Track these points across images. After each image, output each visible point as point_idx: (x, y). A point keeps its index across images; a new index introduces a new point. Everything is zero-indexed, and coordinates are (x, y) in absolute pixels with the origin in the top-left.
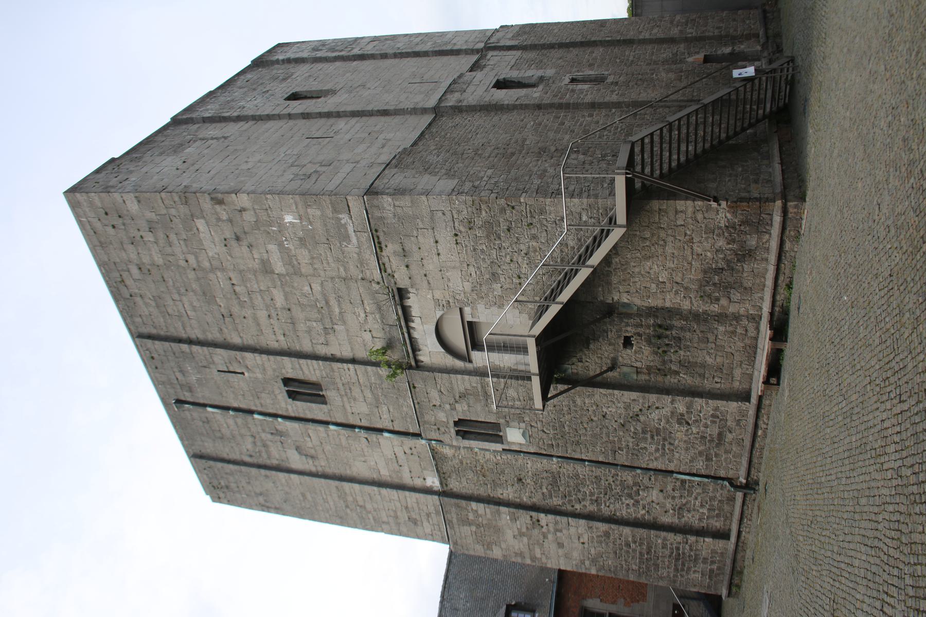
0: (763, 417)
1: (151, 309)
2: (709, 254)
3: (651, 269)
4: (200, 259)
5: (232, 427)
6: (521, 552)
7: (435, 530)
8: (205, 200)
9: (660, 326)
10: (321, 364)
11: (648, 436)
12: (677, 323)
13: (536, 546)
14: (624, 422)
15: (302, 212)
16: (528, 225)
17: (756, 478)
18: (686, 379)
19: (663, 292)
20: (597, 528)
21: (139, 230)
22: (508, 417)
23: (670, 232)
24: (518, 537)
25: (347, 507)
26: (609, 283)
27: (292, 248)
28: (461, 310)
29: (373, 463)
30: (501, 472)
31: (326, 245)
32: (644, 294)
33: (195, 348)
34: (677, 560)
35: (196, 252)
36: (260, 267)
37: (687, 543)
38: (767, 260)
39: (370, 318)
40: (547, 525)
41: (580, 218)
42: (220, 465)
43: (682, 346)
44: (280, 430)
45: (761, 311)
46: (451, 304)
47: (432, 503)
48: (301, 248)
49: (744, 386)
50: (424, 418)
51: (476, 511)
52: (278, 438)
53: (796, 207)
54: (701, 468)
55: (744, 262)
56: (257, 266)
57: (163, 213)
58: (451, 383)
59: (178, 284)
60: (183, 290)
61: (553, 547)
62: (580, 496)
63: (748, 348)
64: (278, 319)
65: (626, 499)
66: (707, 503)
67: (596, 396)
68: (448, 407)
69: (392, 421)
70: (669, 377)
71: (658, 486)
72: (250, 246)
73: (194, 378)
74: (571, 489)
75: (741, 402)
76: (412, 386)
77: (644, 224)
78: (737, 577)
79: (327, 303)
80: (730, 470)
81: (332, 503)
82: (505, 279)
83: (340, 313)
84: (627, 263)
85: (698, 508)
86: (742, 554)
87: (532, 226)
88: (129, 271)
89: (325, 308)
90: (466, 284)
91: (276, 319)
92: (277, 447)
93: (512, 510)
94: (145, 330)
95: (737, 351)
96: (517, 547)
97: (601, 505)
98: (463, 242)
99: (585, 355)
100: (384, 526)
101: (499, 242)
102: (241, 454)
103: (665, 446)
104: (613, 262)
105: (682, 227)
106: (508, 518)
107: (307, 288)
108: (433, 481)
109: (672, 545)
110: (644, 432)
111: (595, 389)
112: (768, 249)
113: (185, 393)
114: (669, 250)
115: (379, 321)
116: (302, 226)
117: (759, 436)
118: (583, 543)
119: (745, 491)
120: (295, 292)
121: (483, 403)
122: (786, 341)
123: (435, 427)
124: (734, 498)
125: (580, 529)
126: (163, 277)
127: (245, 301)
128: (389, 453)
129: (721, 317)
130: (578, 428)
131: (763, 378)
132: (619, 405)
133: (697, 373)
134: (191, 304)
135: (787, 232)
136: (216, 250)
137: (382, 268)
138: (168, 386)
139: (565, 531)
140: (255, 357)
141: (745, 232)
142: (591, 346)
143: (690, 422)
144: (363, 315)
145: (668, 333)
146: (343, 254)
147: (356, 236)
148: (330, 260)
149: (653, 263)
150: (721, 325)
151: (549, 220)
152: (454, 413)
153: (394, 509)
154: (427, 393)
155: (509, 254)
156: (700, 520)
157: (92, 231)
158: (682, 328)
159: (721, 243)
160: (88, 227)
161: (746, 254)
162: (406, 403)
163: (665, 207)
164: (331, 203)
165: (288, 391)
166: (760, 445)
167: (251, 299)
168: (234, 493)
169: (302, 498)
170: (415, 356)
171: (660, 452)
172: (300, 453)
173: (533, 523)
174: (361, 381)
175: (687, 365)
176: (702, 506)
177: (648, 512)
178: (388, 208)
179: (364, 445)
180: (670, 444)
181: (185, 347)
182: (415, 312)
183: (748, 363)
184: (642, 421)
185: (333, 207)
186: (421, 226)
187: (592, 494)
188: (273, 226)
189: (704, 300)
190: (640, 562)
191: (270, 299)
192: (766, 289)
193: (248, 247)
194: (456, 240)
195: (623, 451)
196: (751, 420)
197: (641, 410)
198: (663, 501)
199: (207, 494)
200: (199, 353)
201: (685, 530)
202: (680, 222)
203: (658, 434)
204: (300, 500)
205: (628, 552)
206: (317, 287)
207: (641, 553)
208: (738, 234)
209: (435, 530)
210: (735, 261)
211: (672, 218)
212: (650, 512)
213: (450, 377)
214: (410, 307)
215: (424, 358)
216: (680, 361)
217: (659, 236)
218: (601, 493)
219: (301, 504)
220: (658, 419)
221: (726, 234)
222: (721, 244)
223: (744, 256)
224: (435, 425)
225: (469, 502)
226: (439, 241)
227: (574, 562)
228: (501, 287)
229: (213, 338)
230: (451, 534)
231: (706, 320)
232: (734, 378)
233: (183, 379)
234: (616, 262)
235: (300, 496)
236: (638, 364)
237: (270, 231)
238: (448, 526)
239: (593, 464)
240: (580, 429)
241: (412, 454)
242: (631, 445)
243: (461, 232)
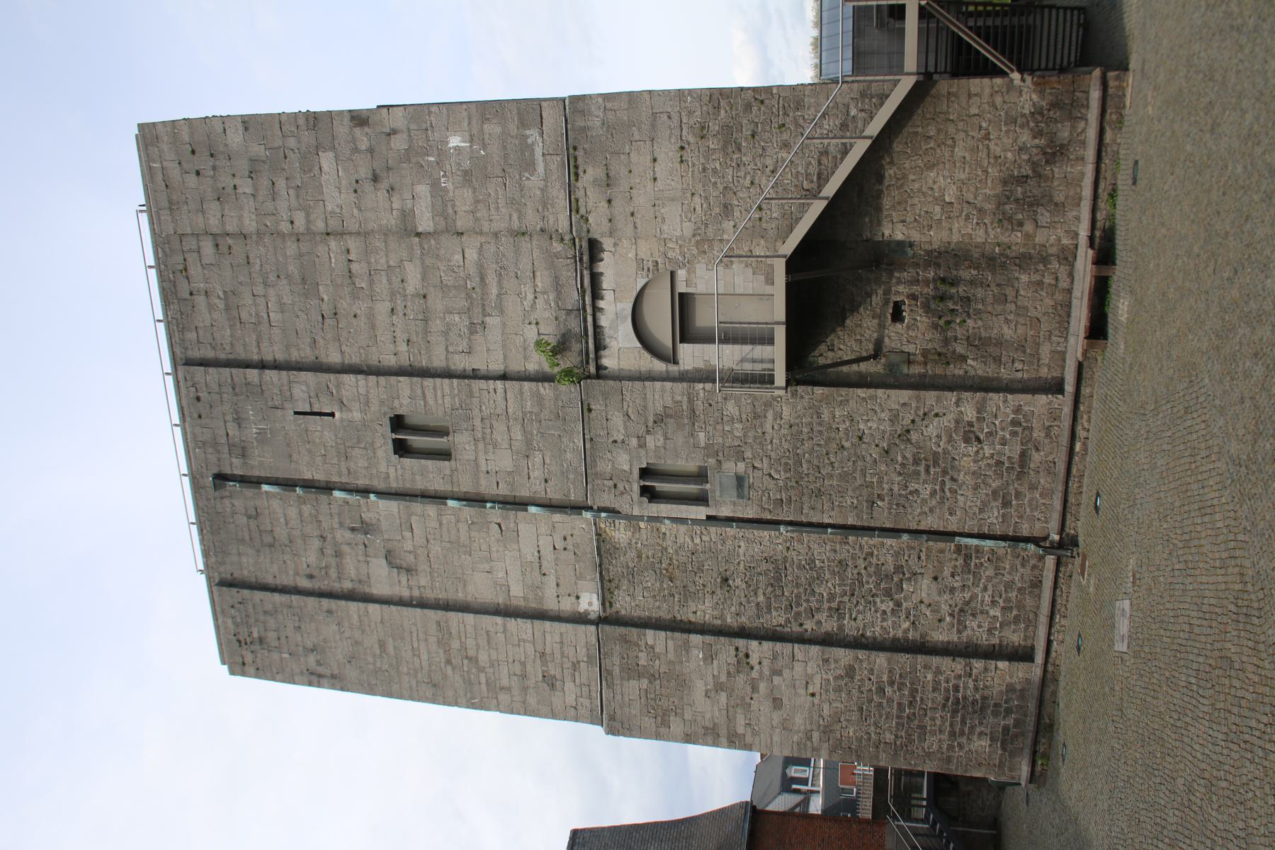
0: (1082, 417)
1: (216, 315)
2: (1009, 155)
3: (935, 182)
4: (313, 217)
6: (714, 724)
7: (581, 697)
8: (342, 120)
9: (943, 280)
11: (922, 468)
12: (966, 274)
15: (475, 131)
16: (779, 128)
17: (1072, 532)
18: (975, 367)
19: (949, 217)
21: (234, 175)
22: (721, 454)
23: (961, 125)
24: (713, 694)
25: (449, 662)
26: (879, 209)
27: (450, 187)
28: (673, 274)
29: (501, 574)
30: (698, 569)
31: (500, 179)
32: (925, 223)
33: (270, 375)
34: (955, 712)
35: (310, 206)
37: (970, 675)
38: (1083, 159)
39: (540, 302)
40: (760, 663)
42: (259, 595)
43: (971, 311)
44: (368, 520)
45: (1077, 239)
46: (660, 266)
48: (464, 186)
49: (1054, 374)
50: (595, 466)
52: (360, 537)
53: (1118, 78)
54: (995, 521)
55: (1055, 163)
56: (393, 222)
57: (277, 145)
58: (645, 398)
60: (272, 278)
61: (766, 707)
62: (814, 605)
63: (1059, 308)
64: (405, 314)
65: (882, 602)
66: (1001, 596)
67: (851, 402)
68: (634, 441)
69: (546, 481)
70: (952, 366)
71: (930, 573)
73: (255, 430)
74: (801, 590)
75: (1052, 394)
76: (585, 408)
77: (928, 116)
78: (1044, 737)
79: (482, 279)
80: (1036, 522)
81: (425, 657)
82: (741, 213)
83: (499, 295)
84: (905, 176)
85: (988, 608)
86: (1052, 687)
87: (784, 129)
88: (199, 252)
89: (477, 290)
91: (401, 314)
92: (357, 555)
93: (709, 639)
94: (196, 354)
95: (1044, 314)
96: (708, 716)
97: (844, 619)
98: (690, 159)
99: (839, 338)
100: (504, 697)
101: (739, 156)
102: (297, 574)
103: (945, 485)
104: (887, 175)
105: (978, 117)
106: (701, 656)
108: (590, 602)
109: (948, 682)
110: (916, 462)
111: (851, 389)
112: (1083, 143)
113: (234, 460)
114: (959, 152)
115: (552, 305)
116: (472, 152)
117: (1078, 453)
118: (813, 695)
119: (1059, 552)
120: (439, 264)
122: (1114, 263)
123: (611, 483)
124: (1041, 581)
125: (810, 664)
126: (248, 257)
127: (362, 288)
128: (529, 552)
129: (1024, 261)
130: (821, 465)
131: (1085, 332)
132: (883, 415)
133: (990, 355)
135: (1108, 117)
136: (339, 201)
137: (574, 206)
138: (210, 450)
139: (786, 673)
141: (1056, 119)
142: (848, 322)
143: (982, 437)
144: (530, 297)
145: (953, 291)
147: (545, 161)
148: (502, 202)
149: (938, 174)
150: (1024, 273)
151: (806, 117)
152: (643, 452)
153: (523, 659)
154: (607, 420)
155: (749, 173)
156: (990, 631)
157: (164, 183)
158: (972, 283)
159: (1025, 137)
160: (159, 177)
161: (1056, 152)
162: (571, 445)
163: (955, 90)
164: (519, 113)
165: (394, 440)
166: (1078, 470)
167: (371, 282)
168: (269, 651)
169: (378, 652)
170: (597, 358)
172: (390, 564)
173: (738, 662)
175: (980, 344)
177: (913, 623)
178: (596, 113)
180: (953, 479)
181: (253, 374)
182: (607, 283)
183: (1059, 334)
184: (913, 441)
185: (519, 119)
186: (637, 137)
187: (832, 597)
188: (431, 155)
189: (1003, 226)
190: (897, 724)
191: (399, 279)
192: (1083, 203)
193: (388, 191)
194: (681, 157)
196: (1066, 423)
197: (913, 421)
198: (937, 598)
199: (223, 662)
200: (272, 383)
201: (969, 651)
202: (974, 110)
203: (936, 463)
204: (374, 656)
205: (880, 704)
206: (472, 255)
207: (900, 704)
208: (1046, 123)
210: (1043, 163)
211: (964, 104)
212: (917, 623)
213: (644, 387)
214: (602, 274)
215: (609, 361)
216: (969, 337)
217: (947, 132)
218: (846, 594)
219: (374, 664)
220: (937, 436)
221: (1032, 124)
222: (1025, 139)
223: (1054, 154)
224: (611, 479)
225: (642, 630)
226: (659, 160)
227: (796, 738)
228: (734, 226)
229: (299, 359)
231: (1003, 266)
232: (1042, 362)
233: (237, 433)
234: (890, 175)
235: (376, 646)
236: (910, 348)
237: (423, 163)
238: (604, 683)
241: (565, 549)
242: (896, 488)
243: (689, 143)
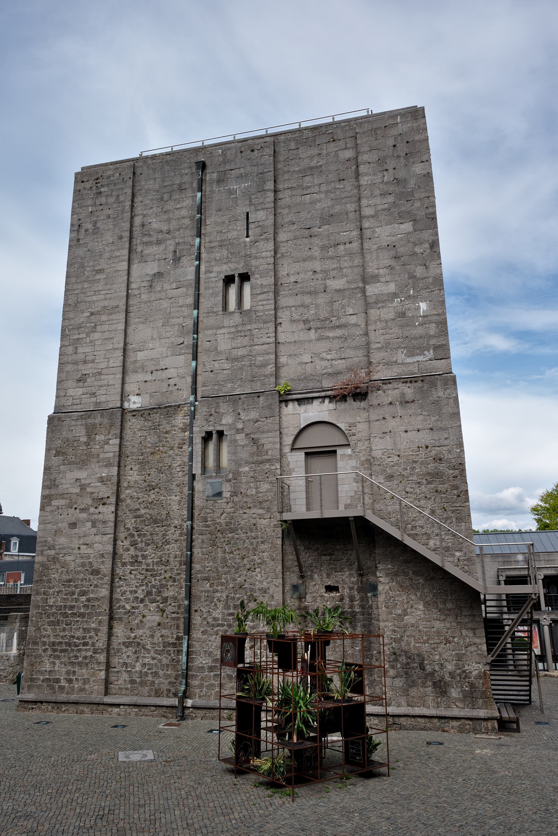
5: (177, 212)
6: (58, 486)
7: (73, 399)
10: (271, 312)
13: (67, 501)
14: (246, 588)
20: (103, 562)
22: (235, 481)
24: (78, 484)
27: (395, 304)
36: (371, 273)
51: (107, 443)
56: (370, 270)
59: (338, 193)
72: (390, 267)
90: (380, 453)
92: (159, 254)
107: (351, 312)
118: (79, 548)
121: (251, 460)
125: (100, 545)
134: (320, 201)
140: (270, 251)
146: (395, 349)
147: (414, 363)
153: (96, 361)
159: (450, 667)
171: (214, 622)
172: (154, 275)
174: (256, 347)
176: (144, 665)
179: (173, 339)
189: (391, 655)
193: (390, 266)
195: (210, 587)
209: (73, 399)
227: (50, 539)
238: (82, 413)
239: (189, 559)
240: (230, 547)
241: (169, 385)
242: (218, 595)
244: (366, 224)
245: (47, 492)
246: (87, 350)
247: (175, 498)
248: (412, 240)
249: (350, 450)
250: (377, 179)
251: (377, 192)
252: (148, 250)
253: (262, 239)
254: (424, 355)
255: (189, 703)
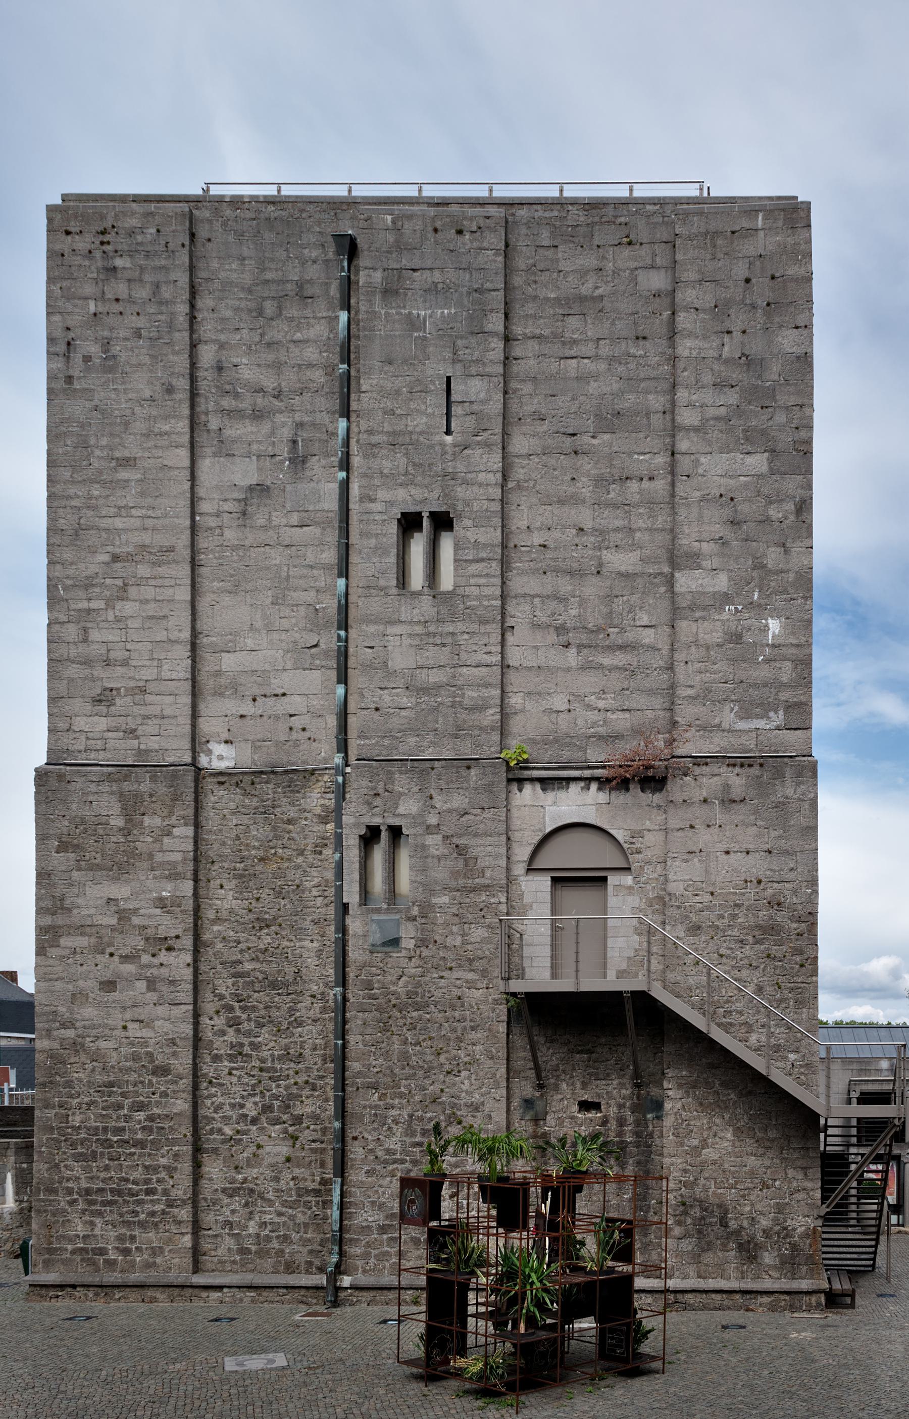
7: (87, 738)
14: (444, 1103)
22: (423, 921)
25: (116, 558)
27: (725, 616)
39: (593, 716)
41: (792, 1051)
47: (168, 746)
69: (377, 709)
90: (681, 886)
107: (645, 620)
114: (752, 1161)
118: (125, 1028)
140: (495, 472)
147: (750, 731)
148: (707, 677)
172: (251, 488)
189: (679, 1206)
193: (721, 538)
230: (680, 762)
241: (291, 729)
244: (683, 445)
245: (48, 920)
246: (111, 638)
247: (311, 944)
248: (765, 490)
249: (630, 877)
250: (710, 348)
251: (708, 378)
252: (237, 430)
253: (478, 443)
254: (769, 718)
255: (346, 1281)
